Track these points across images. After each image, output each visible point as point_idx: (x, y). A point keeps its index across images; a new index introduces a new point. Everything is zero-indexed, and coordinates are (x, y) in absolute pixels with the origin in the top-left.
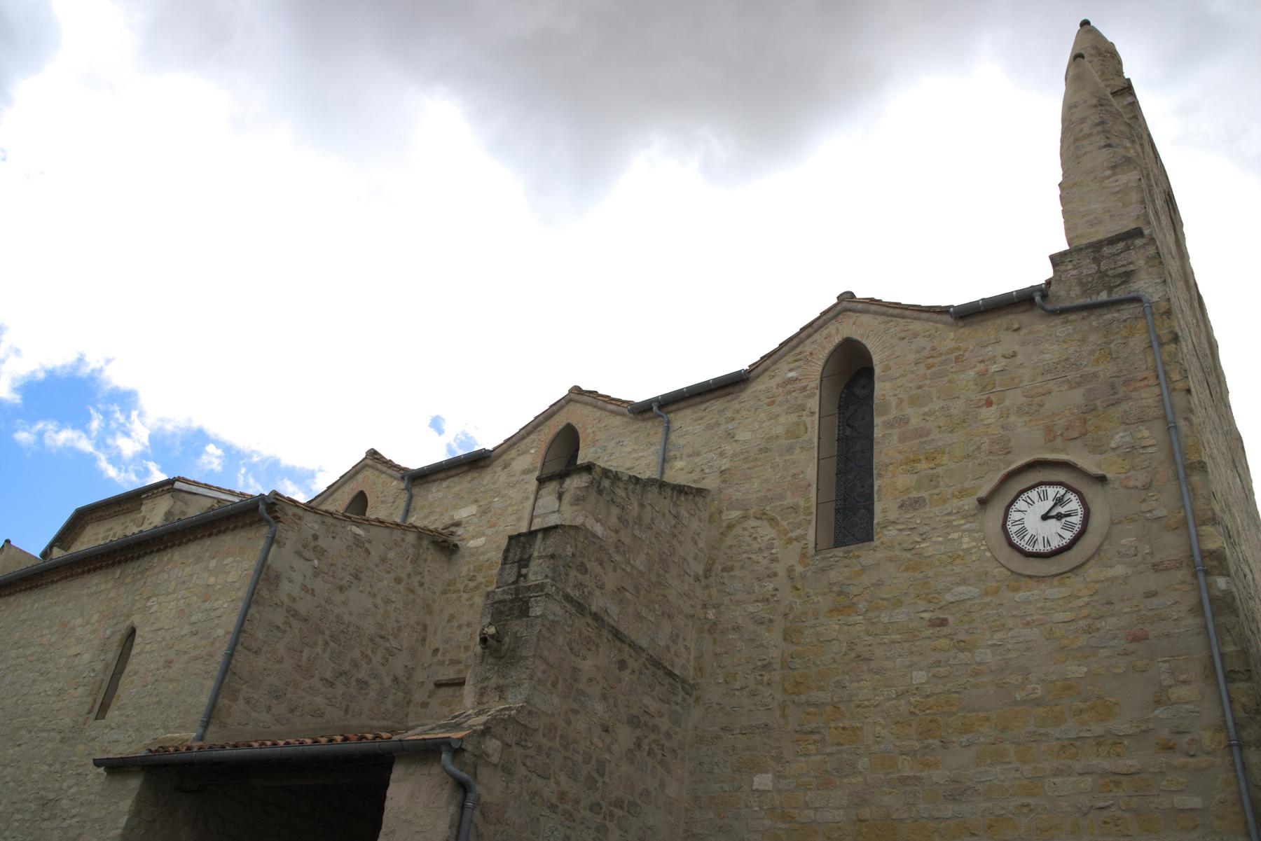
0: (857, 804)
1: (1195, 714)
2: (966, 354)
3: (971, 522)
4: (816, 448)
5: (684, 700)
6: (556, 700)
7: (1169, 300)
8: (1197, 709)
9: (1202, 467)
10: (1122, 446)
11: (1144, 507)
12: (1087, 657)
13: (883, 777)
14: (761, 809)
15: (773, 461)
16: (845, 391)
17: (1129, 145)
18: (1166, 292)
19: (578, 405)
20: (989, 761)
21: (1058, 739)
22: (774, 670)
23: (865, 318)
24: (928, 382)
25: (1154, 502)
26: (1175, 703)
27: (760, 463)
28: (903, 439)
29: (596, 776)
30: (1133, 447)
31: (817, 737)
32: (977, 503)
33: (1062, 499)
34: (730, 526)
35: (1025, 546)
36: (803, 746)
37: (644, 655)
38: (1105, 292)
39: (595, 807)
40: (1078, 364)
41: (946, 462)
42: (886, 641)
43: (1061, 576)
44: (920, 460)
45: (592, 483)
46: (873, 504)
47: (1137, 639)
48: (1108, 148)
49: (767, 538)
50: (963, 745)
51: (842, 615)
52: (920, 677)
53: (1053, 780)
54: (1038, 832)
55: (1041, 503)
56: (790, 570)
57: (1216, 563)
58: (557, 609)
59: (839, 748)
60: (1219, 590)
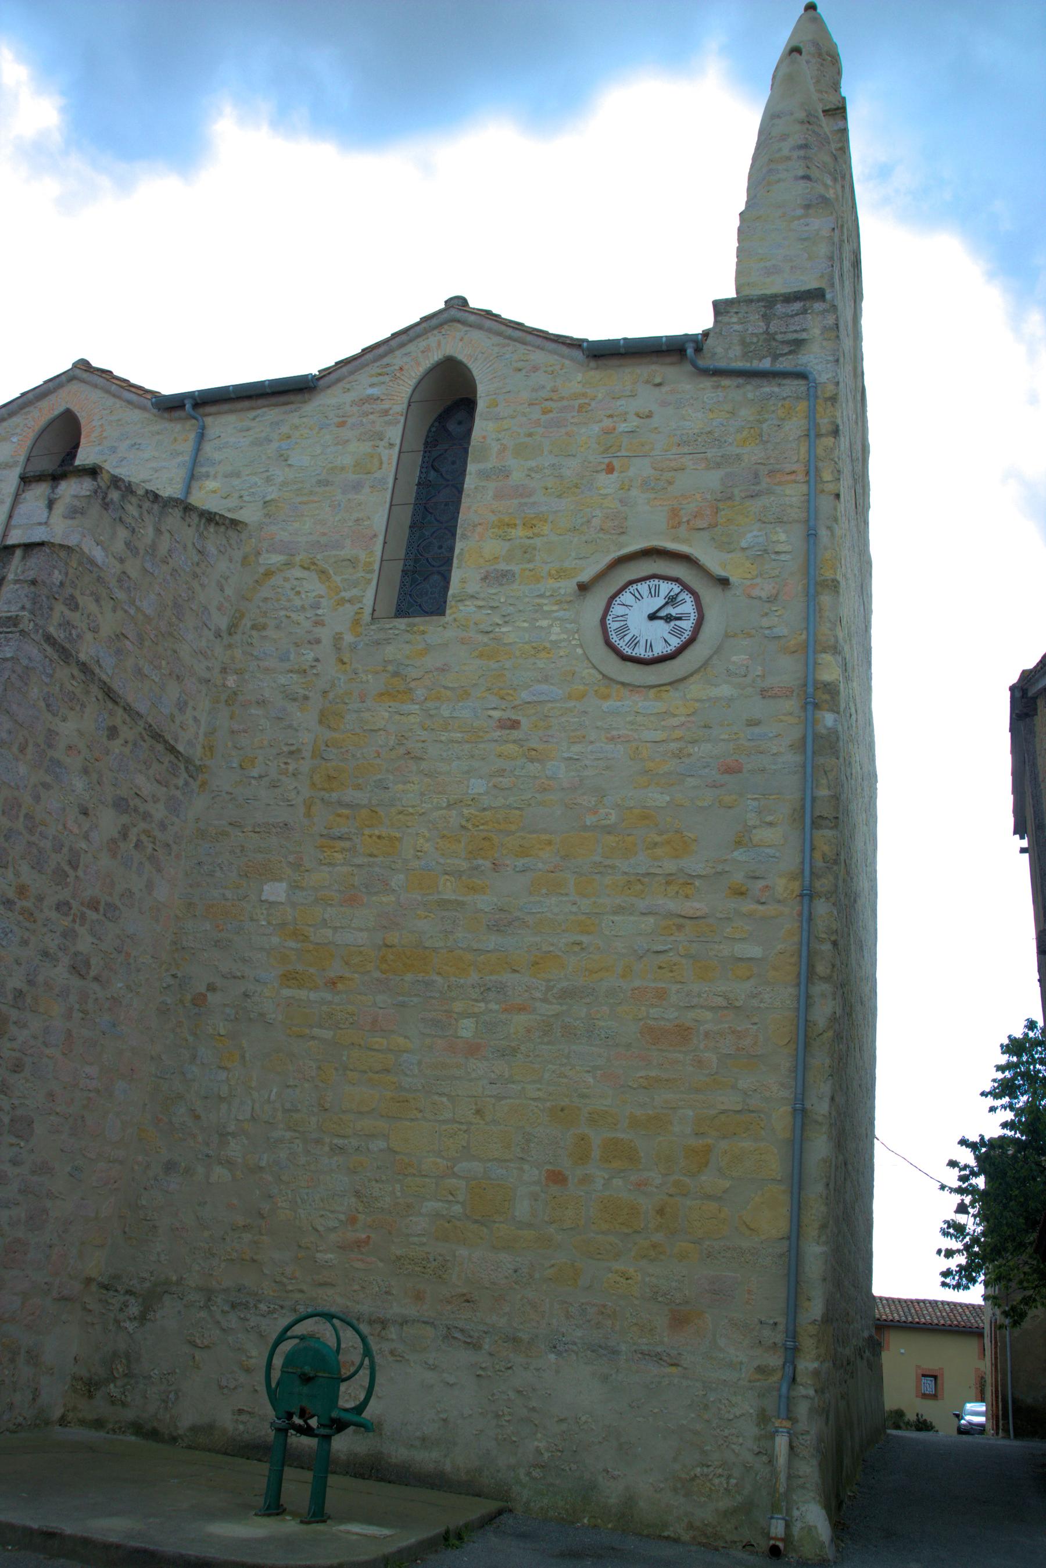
0: (385, 927)
1: (774, 859)
2: (593, 404)
3: (565, 610)
4: (390, 491)
5: (186, 784)
6: (23, 769)
7: (837, 384)
8: (777, 854)
9: (834, 586)
10: (753, 546)
11: (765, 622)
12: (672, 784)
13: (419, 898)
14: (269, 923)
15: (334, 499)
16: (437, 424)
17: (829, 182)
18: (837, 374)
19: (82, 384)
20: (544, 891)
21: (626, 873)
22: (303, 758)
23: (476, 335)
24: (541, 430)
25: (776, 619)
26: (755, 846)
27: (316, 499)
28: (499, 496)
29: (67, 868)
30: (765, 550)
31: (347, 844)
32: (576, 587)
33: (675, 598)
34: (268, 574)
35: (624, 647)
36: (329, 853)
37: (141, 723)
38: (769, 359)
39: (62, 907)
40: (723, 440)
41: (546, 532)
42: (443, 738)
43: (659, 689)
44: (515, 525)
45: (96, 492)
46: (450, 571)
47: (730, 770)
48: (805, 181)
49: (314, 594)
50: (518, 869)
51: (394, 701)
52: (478, 786)
53: (612, 918)
54: (587, 973)
55: (651, 600)
56: (338, 638)
57: (827, 697)
58: (34, 652)
59: (372, 859)
60: (825, 726)
